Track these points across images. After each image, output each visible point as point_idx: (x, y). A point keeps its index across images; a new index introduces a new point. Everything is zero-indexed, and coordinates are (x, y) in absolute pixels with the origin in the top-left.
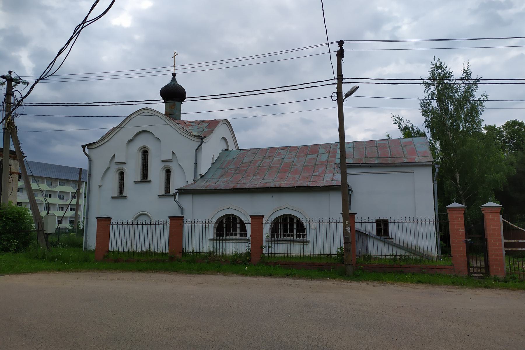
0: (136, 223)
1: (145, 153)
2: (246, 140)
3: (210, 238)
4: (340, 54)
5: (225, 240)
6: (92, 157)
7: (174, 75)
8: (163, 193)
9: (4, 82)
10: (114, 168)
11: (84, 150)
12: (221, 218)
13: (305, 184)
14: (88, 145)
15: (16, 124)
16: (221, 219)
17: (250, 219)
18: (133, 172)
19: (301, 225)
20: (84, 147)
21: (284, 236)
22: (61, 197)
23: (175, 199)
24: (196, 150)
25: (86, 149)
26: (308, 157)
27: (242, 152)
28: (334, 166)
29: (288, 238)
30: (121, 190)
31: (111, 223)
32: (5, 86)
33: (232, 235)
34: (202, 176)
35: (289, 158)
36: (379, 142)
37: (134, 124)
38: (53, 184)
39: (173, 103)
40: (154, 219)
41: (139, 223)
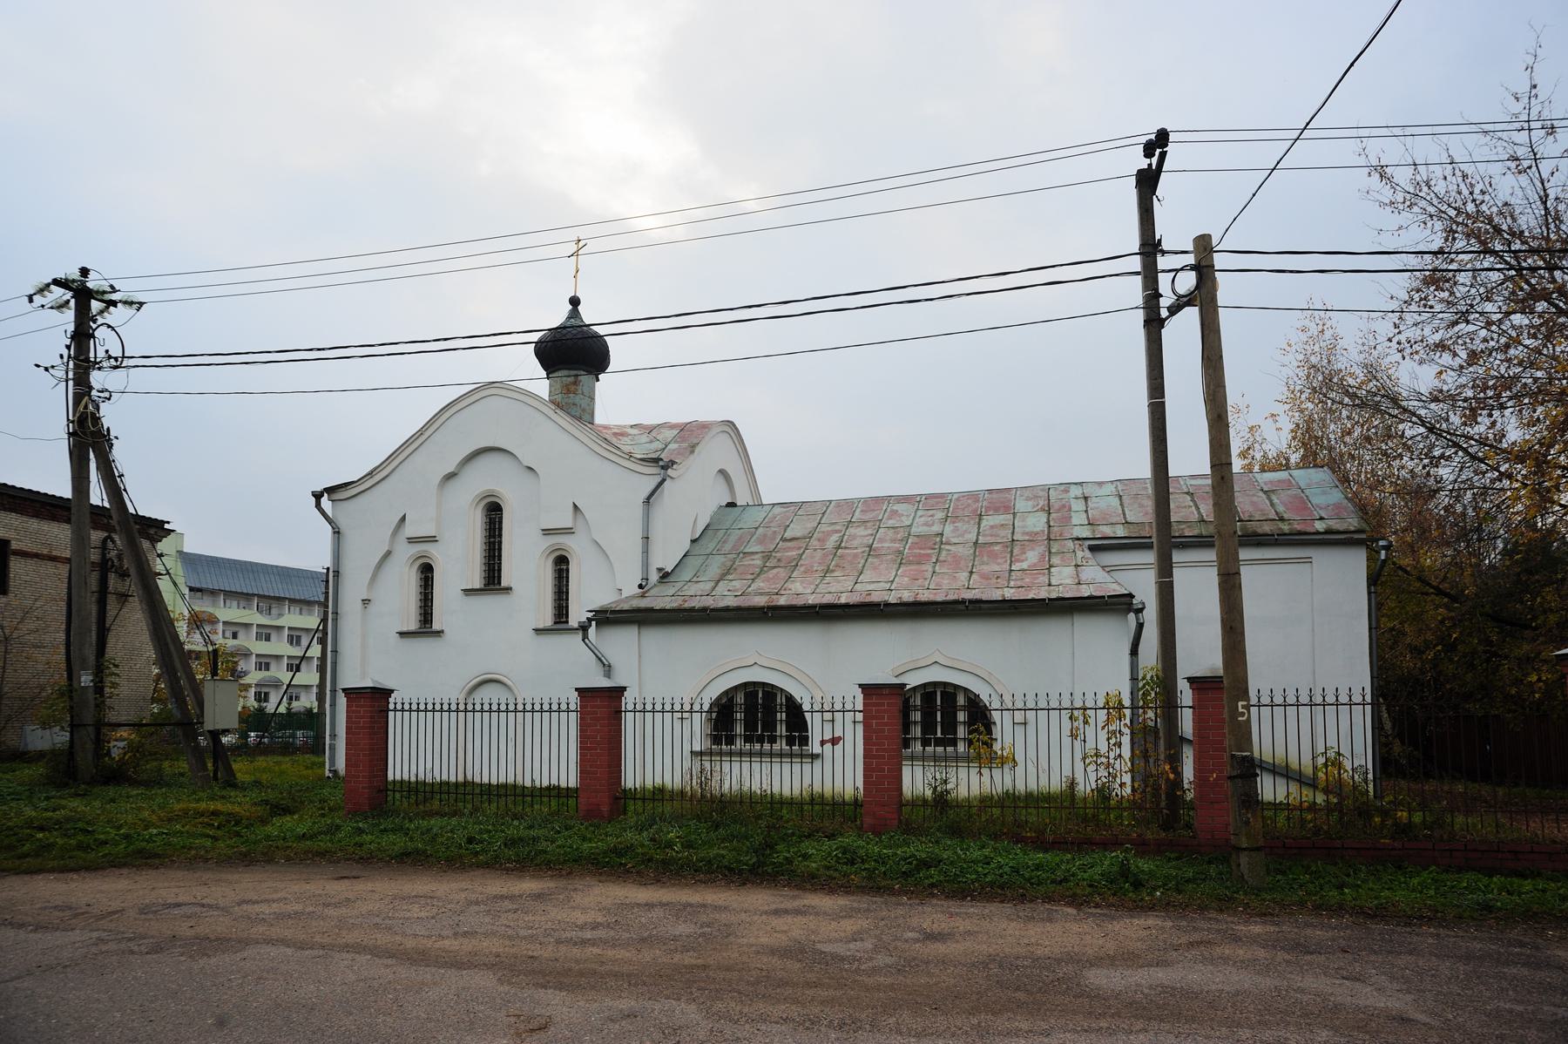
0: (470, 707)
1: (494, 512)
2: (783, 478)
3: (697, 748)
4: (1147, 182)
5: (741, 754)
6: (343, 523)
7: (575, 302)
8: (547, 620)
9: (68, 302)
10: (405, 554)
11: (318, 505)
12: (726, 692)
13: (996, 595)
14: (330, 490)
15: (106, 423)
16: (730, 694)
17: (860, 697)
18: (459, 564)
19: (980, 715)
20: (318, 496)
21: (925, 743)
22: (294, 640)
23: (585, 637)
24: (648, 500)
25: (325, 501)
26: (984, 523)
27: (777, 510)
28: (1070, 544)
29: (940, 749)
30: (426, 615)
31: (391, 706)
32: (70, 315)
33: (761, 740)
34: (665, 576)
35: (1485, 340)
36: (1194, 482)
37: (459, 439)
38: (274, 611)
39: (571, 379)
40: (526, 693)
41: (478, 707)
